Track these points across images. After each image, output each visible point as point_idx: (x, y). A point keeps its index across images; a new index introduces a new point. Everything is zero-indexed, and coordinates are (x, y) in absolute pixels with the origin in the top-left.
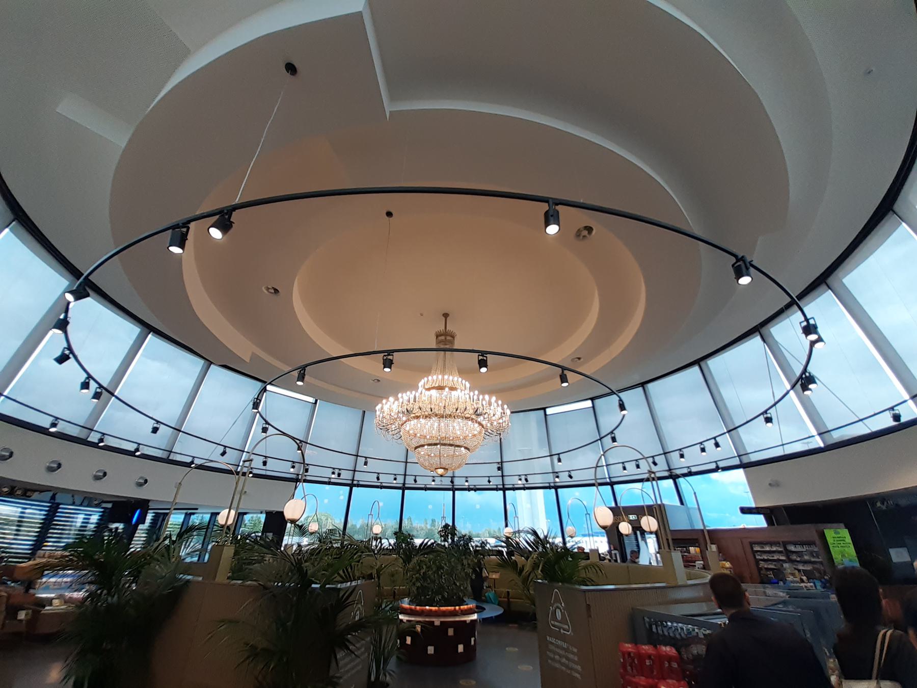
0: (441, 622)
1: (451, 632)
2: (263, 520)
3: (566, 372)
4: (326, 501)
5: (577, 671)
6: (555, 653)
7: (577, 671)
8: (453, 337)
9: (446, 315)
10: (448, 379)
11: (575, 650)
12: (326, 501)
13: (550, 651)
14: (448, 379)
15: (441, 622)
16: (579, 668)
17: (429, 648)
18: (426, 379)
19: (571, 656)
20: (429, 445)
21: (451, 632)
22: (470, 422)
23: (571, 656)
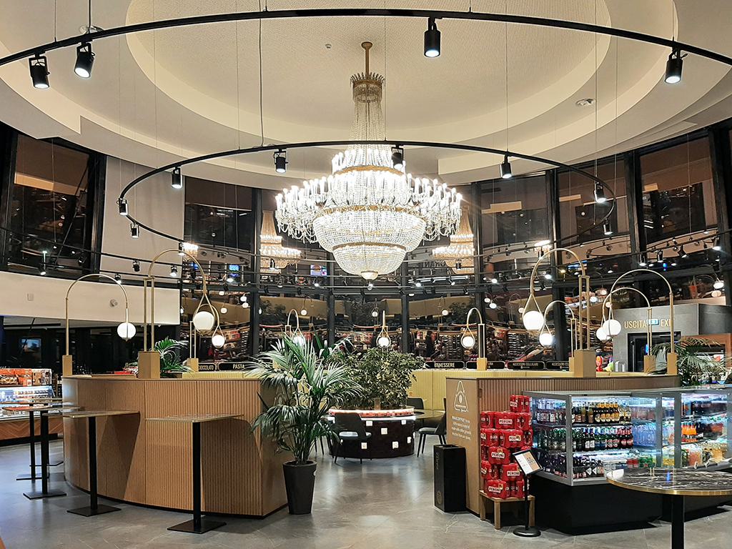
0: (407, 421)
1: (384, 431)
2: (725, 300)
3: (510, 159)
4: (304, 312)
5: (468, 435)
6: (456, 427)
7: (468, 435)
8: (379, 84)
9: (367, 46)
10: (372, 155)
11: (469, 422)
12: (304, 312)
13: (454, 426)
14: (372, 155)
15: (407, 421)
16: (470, 433)
17: (362, 444)
18: (341, 155)
19: (466, 426)
20: (351, 245)
21: (384, 431)
22: (404, 214)
23: (466, 426)
